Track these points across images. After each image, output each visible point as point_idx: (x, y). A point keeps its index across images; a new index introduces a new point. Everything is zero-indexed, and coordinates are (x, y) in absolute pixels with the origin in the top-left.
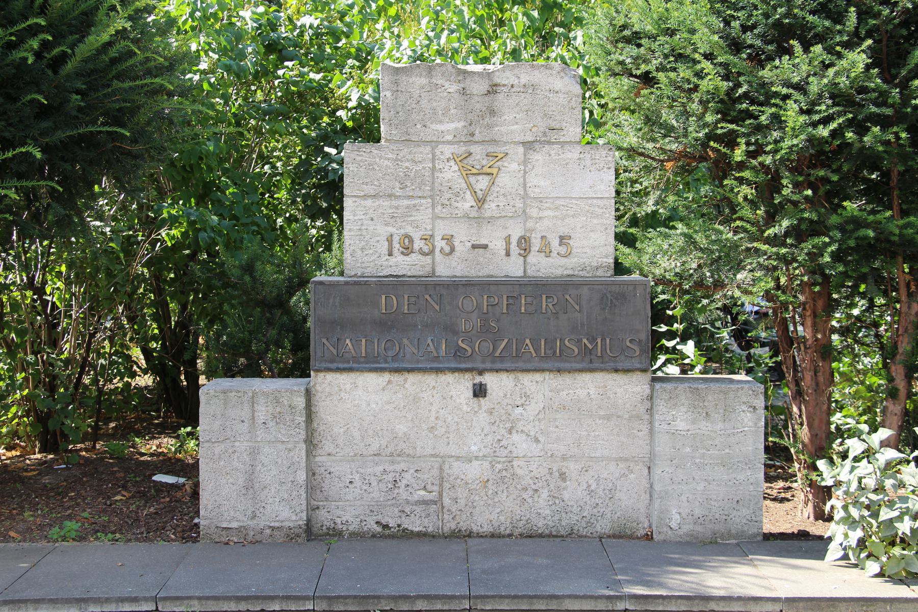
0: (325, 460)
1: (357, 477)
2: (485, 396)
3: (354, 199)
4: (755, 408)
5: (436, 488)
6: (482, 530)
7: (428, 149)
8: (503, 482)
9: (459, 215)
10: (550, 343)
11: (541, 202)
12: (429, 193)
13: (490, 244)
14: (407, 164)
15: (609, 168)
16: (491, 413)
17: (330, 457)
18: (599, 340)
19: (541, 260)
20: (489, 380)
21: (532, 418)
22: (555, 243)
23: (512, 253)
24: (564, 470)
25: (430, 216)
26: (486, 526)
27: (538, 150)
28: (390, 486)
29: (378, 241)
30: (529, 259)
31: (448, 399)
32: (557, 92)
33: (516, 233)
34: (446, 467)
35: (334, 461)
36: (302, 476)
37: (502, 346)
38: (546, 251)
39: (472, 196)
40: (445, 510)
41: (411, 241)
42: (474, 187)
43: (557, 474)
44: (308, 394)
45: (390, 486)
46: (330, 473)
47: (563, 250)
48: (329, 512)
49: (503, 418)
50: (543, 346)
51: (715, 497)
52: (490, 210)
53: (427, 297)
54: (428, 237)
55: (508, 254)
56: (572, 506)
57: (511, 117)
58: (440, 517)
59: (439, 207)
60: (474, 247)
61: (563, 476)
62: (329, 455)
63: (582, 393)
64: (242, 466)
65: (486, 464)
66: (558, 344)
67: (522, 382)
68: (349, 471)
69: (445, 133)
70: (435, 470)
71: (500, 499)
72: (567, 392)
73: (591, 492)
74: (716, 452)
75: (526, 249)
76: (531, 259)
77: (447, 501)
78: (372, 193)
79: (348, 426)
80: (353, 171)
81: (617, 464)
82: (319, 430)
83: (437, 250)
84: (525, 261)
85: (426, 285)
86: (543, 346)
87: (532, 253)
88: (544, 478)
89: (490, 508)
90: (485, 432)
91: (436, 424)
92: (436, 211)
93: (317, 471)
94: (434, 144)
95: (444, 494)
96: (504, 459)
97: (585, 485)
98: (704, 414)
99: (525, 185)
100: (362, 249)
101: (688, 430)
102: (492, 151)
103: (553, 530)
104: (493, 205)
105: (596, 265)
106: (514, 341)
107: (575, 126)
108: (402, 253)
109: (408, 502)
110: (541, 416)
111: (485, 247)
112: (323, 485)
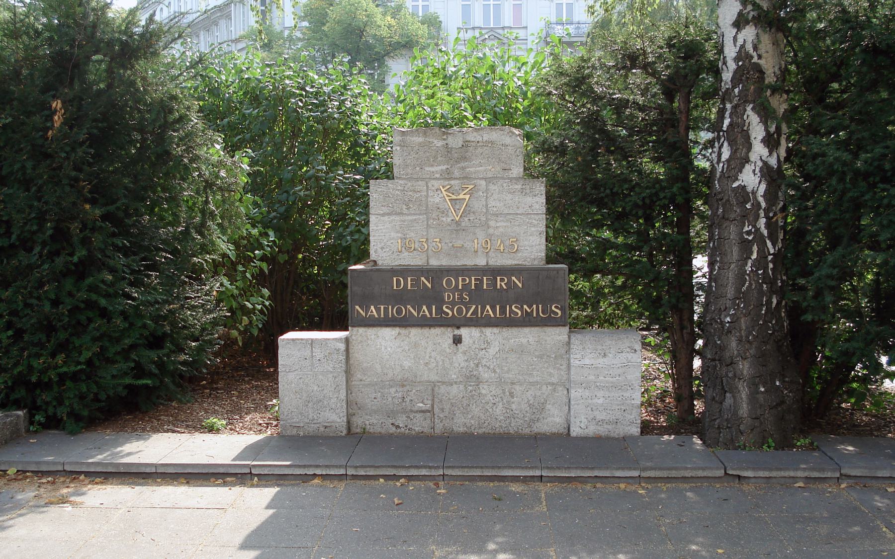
4: (635, 351)
5: (430, 402)
14: (410, 193)
18: (534, 306)
34: (436, 389)
40: (436, 416)
43: (508, 393)
59: (432, 221)
61: (512, 395)
65: (462, 387)
77: (436, 410)
90: (461, 365)
99: (487, 205)
100: (382, 248)
109: (412, 411)
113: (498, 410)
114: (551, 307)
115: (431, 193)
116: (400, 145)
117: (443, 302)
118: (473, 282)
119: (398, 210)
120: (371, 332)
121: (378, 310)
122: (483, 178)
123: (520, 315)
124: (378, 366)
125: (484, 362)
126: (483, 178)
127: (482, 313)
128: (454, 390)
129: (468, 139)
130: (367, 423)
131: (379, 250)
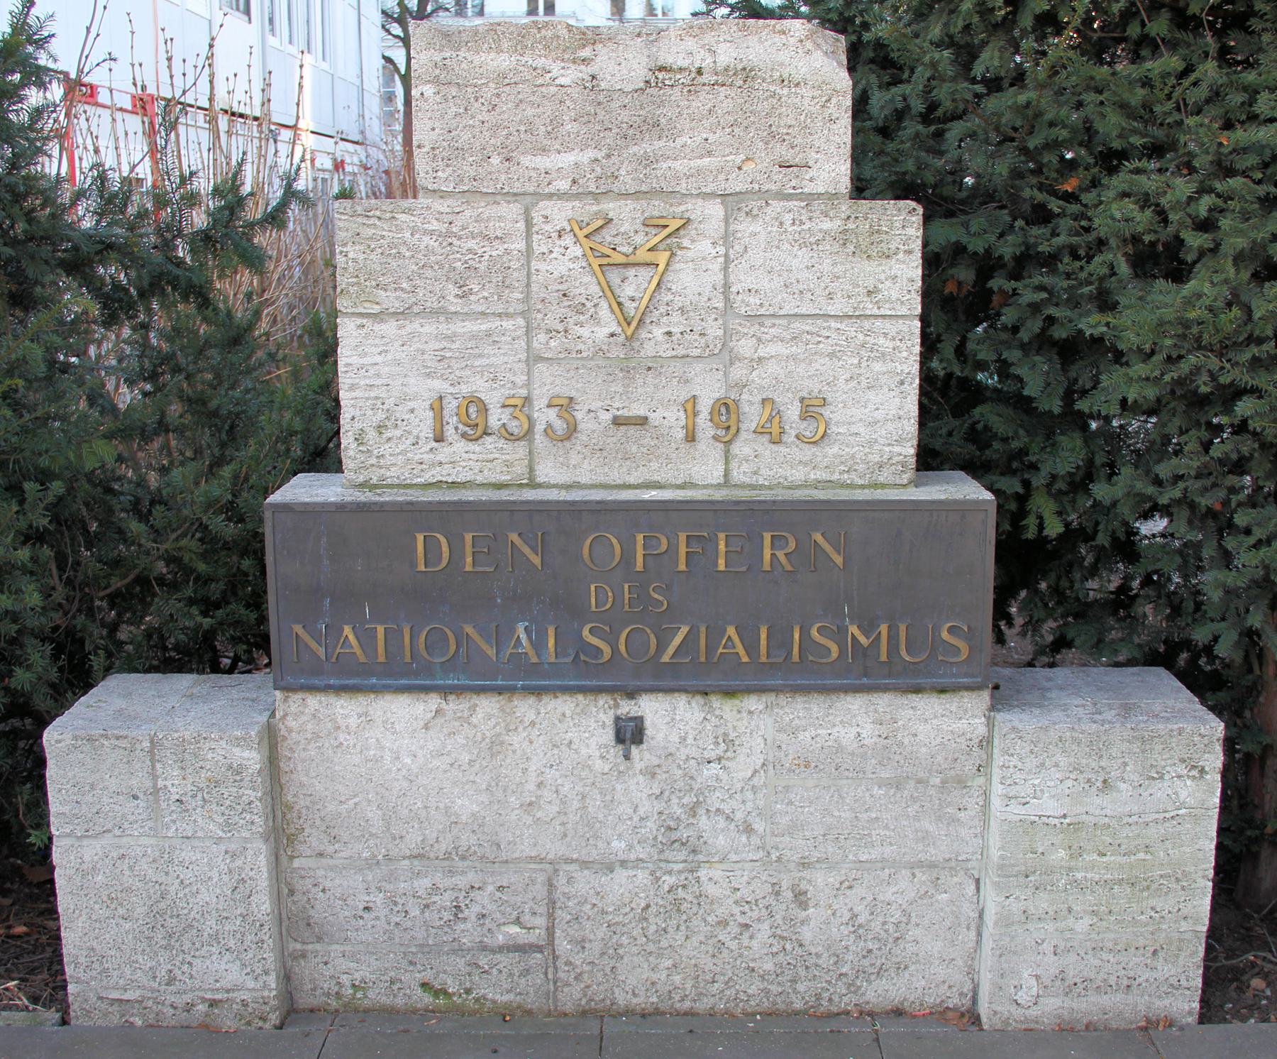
0: (314, 866)
1: (379, 899)
2: (641, 742)
3: (359, 321)
4: (1202, 771)
5: (541, 921)
6: (635, 1001)
7: (512, 211)
8: (679, 910)
9: (585, 355)
10: (780, 640)
11: (761, 324)
12: (520, 307)
13: (651, 416)
14: (471, 244)
15: (910, 252)
16: (653, 775)
17: (324, 861)
18: (884, 629)
19: (760, 449)
20: (651, 708)
21: (739, 786)
22: (793, 412)
23: (699, 435)
24: (803, 886)
25: (523, 356)
26: (642, 993)
27: (755, 212)
28: (447, 916)
29: (412, 411)
30: (736, 448)
31: (563, 748)
32: (797, 85)
33: (708, 391)
34: (561, 881)
35: (332, 868)
36: (263, 905)
37: (677, 640)
38: (772, 432)
39: (612, 311)
40: (560, 963)
41: (484, 409)
42: (617, 292)
43: (790, 895)
44: (272, 739)
45: (447, 916)
46: (324, 891)
47: (808, 429)
48: (326, 963)
49: (680, 784)
50: (763, 642)
51: (1110, 945)
52: (652, 343)
53: (514, 537)
54: (519, 402)
55: (691, 437)
56: (818, 956)
57: (698, 139)
58: (550, 976)
59: (542, 337)
60: (617, 422)
61: (801, 898)
62: (321, 855)
63: (846, 735)
64: (140, 884)
65: (642, 876)
66: (797, 636)
67: (718, 712)
68: (361, 886)
69: (554, 175)
70: (538, 886)
71: (673, 943)
72: (813, 733)
73: (858, 931)
74: (1119, 859)
75: (728, 428)
76: (741, 448)
77: (563, 946)
78: (397, 306)
79: (357, 800)
80: (355, 260)
81: (914, 875)
82: (297, 807)
83: (540, 428)
84: (727, 452)
85: (510, 509)
86: (763, 642)
87: (743, 435)
88: (765, 902)
89: (651, 959)
90: (641, 812)
91: (539, 797)
92: (535, 344)
93: (298, 887)
94: (529, 199)
95: (558, 933)
96: (681, 866)
97: (847, 915)
98: (1099, 784)
99: (727, 286)
100: (380, 428)
101: (1065, 816)
102: (656, 213)
103: (779, 1000)
104: (658, 332)
105: (877, 459)
106: (703, 629)
107: (836, 159)
108: (464, 435)
109: (484, 948)
110: (759, 780)
111: (643, 421)
112: (312, 912)
113: (755, 944)
114: (936, 629)
115: (539, 246)
116: (436, 81)
117: (578, 613)
118: (683, 550)
119: (432, 303)
120: (345, 709)
121: (367, 639)
122: (713, 195)
123: (835, 654)
124: (373, 814)
125: (714, 800)
126: (713, 195)
127: (710, 649)
128: (620, 884)
129: (668, 59)
130: (345, 979)
131: (371, 435)
